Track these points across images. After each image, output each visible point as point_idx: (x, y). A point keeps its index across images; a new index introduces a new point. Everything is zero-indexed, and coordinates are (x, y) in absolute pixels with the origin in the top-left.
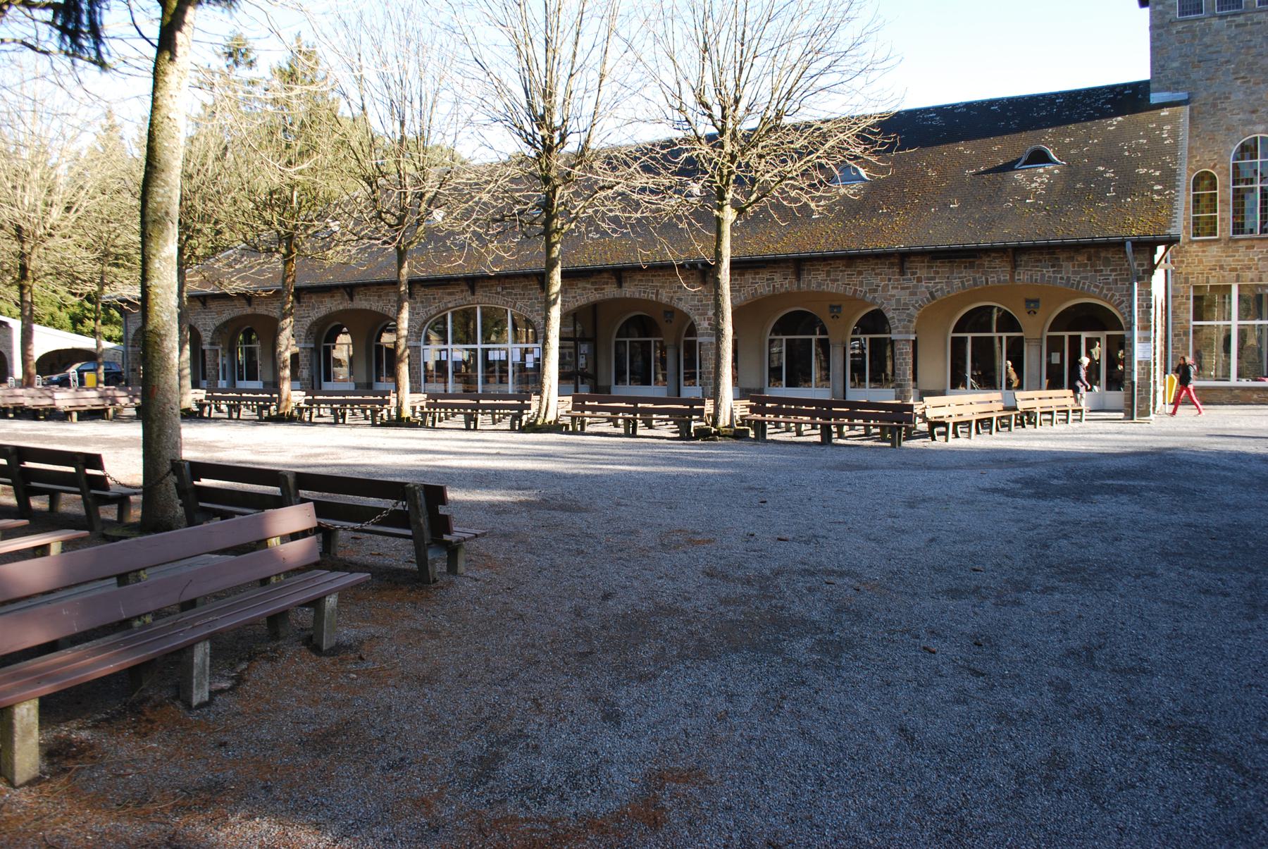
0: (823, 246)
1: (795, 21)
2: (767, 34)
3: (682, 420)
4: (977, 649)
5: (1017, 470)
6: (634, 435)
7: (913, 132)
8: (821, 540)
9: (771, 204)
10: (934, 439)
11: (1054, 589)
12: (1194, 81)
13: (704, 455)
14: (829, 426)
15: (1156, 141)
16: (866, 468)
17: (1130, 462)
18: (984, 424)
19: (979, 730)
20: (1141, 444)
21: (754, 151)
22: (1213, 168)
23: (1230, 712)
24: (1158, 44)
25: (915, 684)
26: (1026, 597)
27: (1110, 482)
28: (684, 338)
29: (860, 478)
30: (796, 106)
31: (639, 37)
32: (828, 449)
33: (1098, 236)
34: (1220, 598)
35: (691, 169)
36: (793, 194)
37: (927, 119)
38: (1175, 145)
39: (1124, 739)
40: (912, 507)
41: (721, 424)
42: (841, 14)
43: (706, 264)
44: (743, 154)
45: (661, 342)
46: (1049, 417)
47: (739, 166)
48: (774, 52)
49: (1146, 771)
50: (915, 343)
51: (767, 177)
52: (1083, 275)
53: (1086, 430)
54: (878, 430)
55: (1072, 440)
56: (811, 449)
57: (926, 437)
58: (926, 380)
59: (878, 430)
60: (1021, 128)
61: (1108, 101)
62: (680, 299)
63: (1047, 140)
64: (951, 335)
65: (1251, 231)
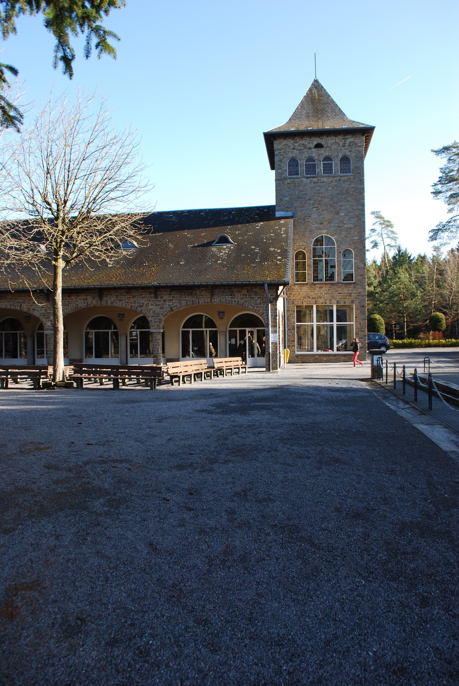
0: (114, 282)
1: (98, 162)
2: (82, 167)
3: (35, 378)
4: (190, 496)
5: (214, 400)
6: (7, 388)
7: (160, 224)
8: (111, 443)
9: (85, 259)
10: (173, 385)
11: (229, 461)
12: (295, 207)
13: (47, 398)
14: (117, 379)
15: (279, 235)
16: (137, 402)
17: (268, 393)
18: (198, 375)
19: (190, 540)
20: (273, 384)
21: (75, 230)
22: (304, 249)
23: (309, 517)
24: (279, 188)
25: (158, 519)
26: (215, 466)
27: (257, 404)
28: (36, 332)
29: (133, 407)
30: (98, 207)
31: (9, 162)
32: (117, 392)
33: (252, 281)
34: (306, 460)
35: (40, 237)
36: (97, 254)
37: (169, 218)
38: (287, 237)
39: (260, 536)
40: (160, 422)
41: (57, 380)
42: (122, 160)
43: (48, 290)
44: (69, 231)
45: (24, 333)
46: (230, 371)
47: (66, 238)
48: (86, 177)
49: (270, 551)
50: (163, 334)
51: (82, 244)
52: (245, 300)
53: (248, 377)
54: (144, 381)
55: (241, 383)
56: (107, 392)
57: (168, 383)
58: (170, 352)
59: (144, 381)
60: (215, 225)
61: (257, 214)
62: (34, 310)
63: (228, 231)
64: (181, 329)
65: (321, 280)
